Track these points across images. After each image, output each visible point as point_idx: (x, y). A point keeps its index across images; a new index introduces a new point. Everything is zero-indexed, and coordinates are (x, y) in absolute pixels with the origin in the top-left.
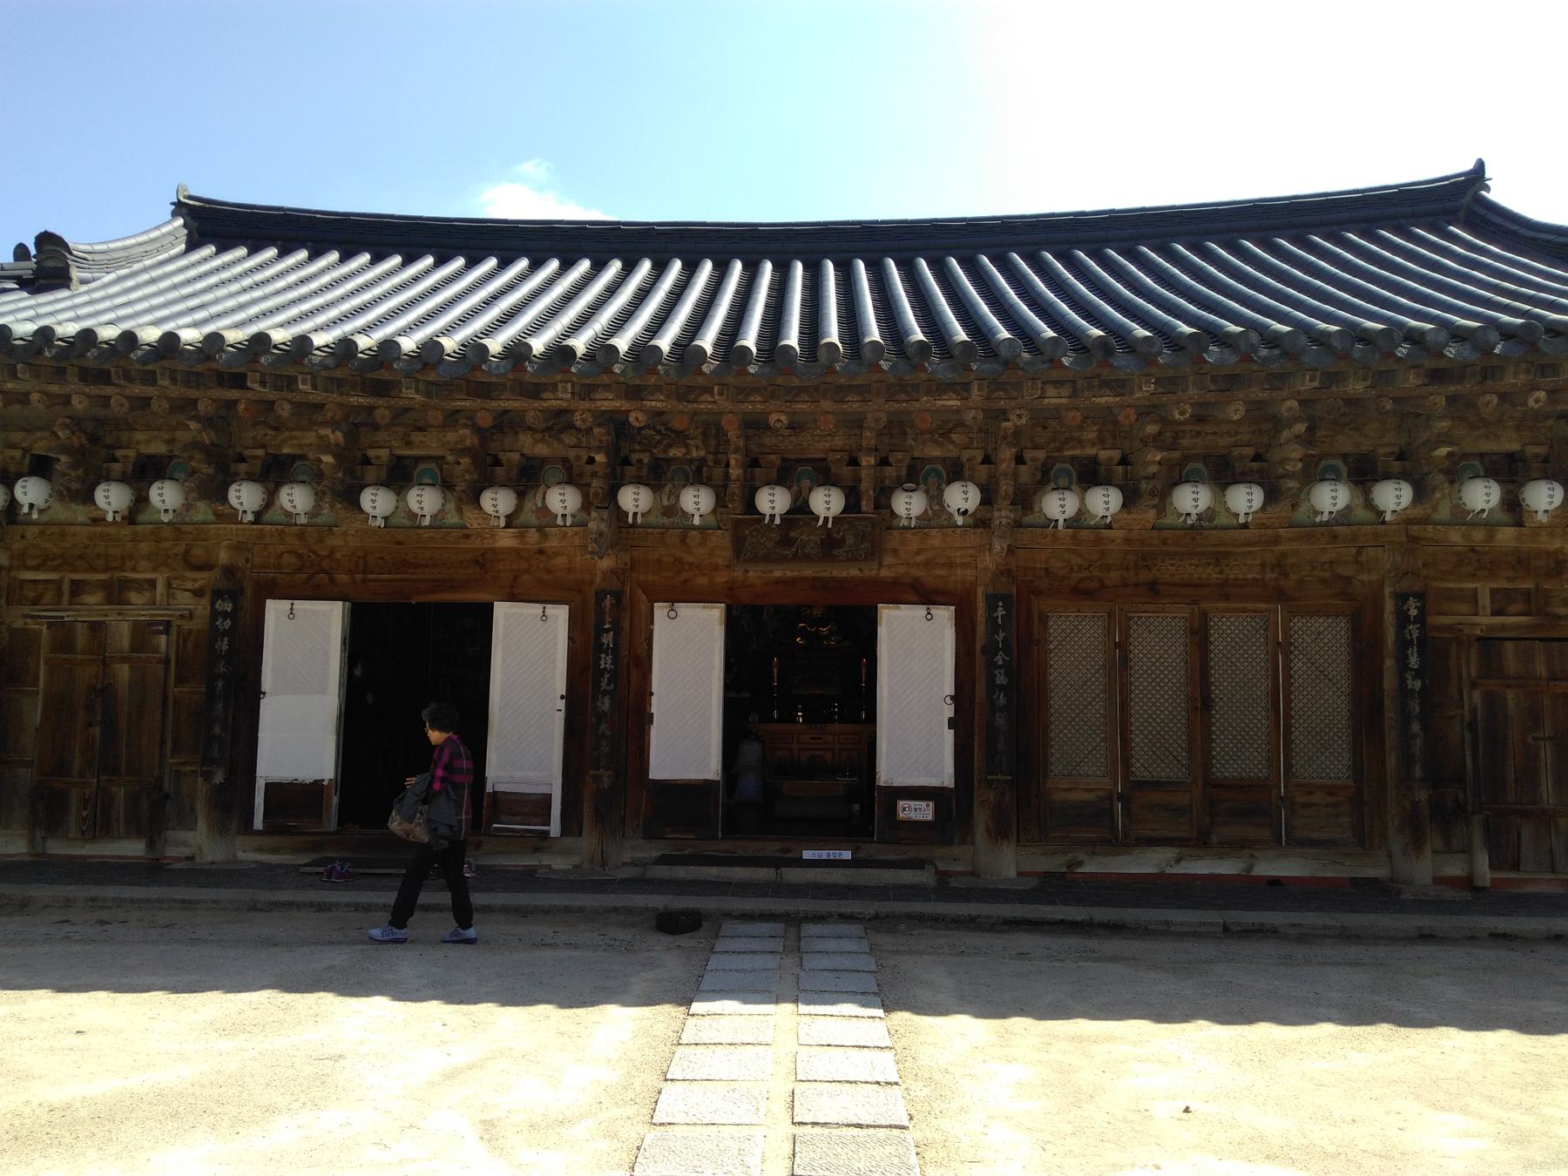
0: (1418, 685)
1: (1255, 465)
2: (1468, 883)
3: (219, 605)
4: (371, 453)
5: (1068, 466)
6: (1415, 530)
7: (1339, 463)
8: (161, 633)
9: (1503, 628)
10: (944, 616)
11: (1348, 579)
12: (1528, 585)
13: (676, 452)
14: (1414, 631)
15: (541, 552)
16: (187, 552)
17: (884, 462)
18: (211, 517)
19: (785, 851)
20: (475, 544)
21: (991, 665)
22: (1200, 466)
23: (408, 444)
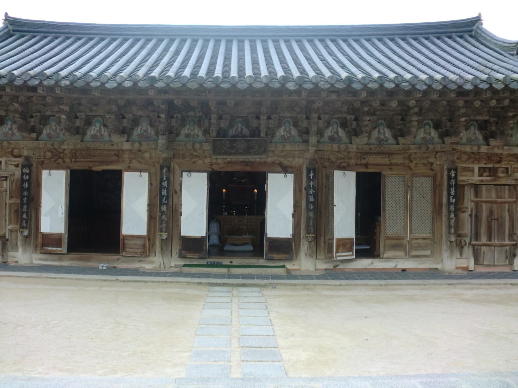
0: (454, 201)
1: (402, 122)
2: (466, 269)
3: (24, 170)
4: (78, 114)
5: (337, 120)
6: (454, 146)
7: (430, 122)
8: (3, 180)
9: (482, 181)
10: (290, 177)
11: (432, 164)
12: (490, 166)
13: (191, 113)
14: (453, 182)
15: (140, 151)
16: (12, 151)
17: (269, 118)
18: (20, 137)
19: (231, 262)
20: (115, 147)
21: (308, 194)
22: (383, 121)
23: (91, 111)
